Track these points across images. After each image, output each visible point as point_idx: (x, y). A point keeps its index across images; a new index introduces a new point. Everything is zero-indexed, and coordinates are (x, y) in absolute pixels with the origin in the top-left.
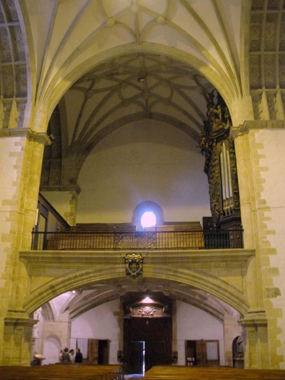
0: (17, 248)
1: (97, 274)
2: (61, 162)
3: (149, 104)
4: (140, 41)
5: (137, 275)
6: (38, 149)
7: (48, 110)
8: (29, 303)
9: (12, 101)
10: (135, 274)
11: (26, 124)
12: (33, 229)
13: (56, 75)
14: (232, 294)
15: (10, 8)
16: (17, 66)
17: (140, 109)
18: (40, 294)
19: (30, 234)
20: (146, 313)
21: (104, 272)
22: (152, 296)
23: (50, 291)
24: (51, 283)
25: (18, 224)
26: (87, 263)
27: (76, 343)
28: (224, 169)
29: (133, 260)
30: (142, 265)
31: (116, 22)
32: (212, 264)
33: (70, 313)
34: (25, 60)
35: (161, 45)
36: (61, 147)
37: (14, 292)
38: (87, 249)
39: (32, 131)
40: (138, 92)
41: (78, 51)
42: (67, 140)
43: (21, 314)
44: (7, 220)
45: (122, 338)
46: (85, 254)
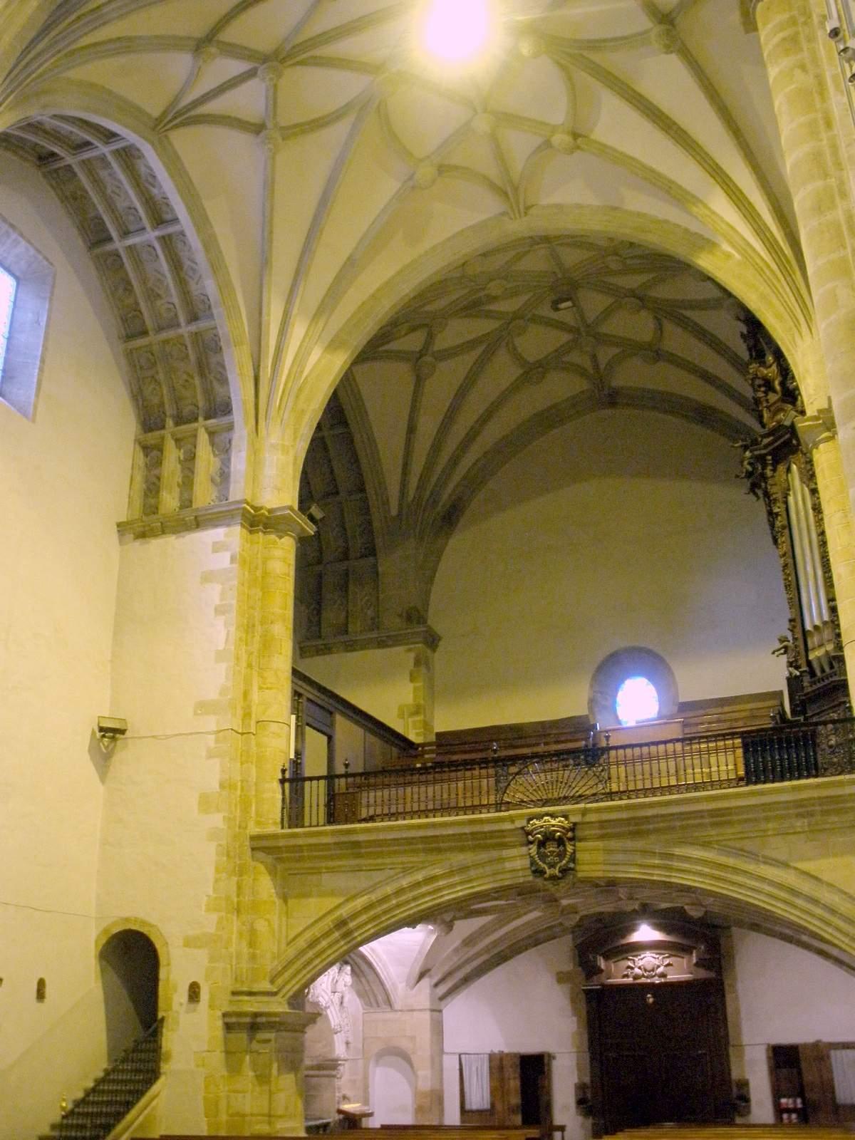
0: (243, 827)
1: (457, 879)
2: (375, 566)
3: (602, 367)
4: (522, 207)
5: (560, 875)
6: (278, 553)
7: (295, 438)
8: (285, 968)
9: (196, 430)
10: (556, 871)
11: (238, 491)
12: (283, 771)
13: (303, 341)
14: (833, 911)
15: (155, 191)
16: (196, 336)
17: (578, 385)
18: (312, 945)
19: (277, 786)
20: (646, 970)
21: (473, 873)
22: (655, 921)
23: (337, 934)
24: (337, 913)
25: (242, 764)
26: (426, 851)
27: (458, 1067)
28: (801, 540)
29: (545, 833)
30: (574, 845)
31: (442, 169)
32: (770, 825)
33: (436, 985)
34: (211, 316)
35: (579, 206)
36: (370, 523)
37: (244, 944)
38: (434, 811)
39: (252, 507)
40: (565, 337)
41: (351, 268)
42: (386, 503)
43: (265, 999)
44: (210, 756)
45: (586, 1044)
46: (419, 827)
